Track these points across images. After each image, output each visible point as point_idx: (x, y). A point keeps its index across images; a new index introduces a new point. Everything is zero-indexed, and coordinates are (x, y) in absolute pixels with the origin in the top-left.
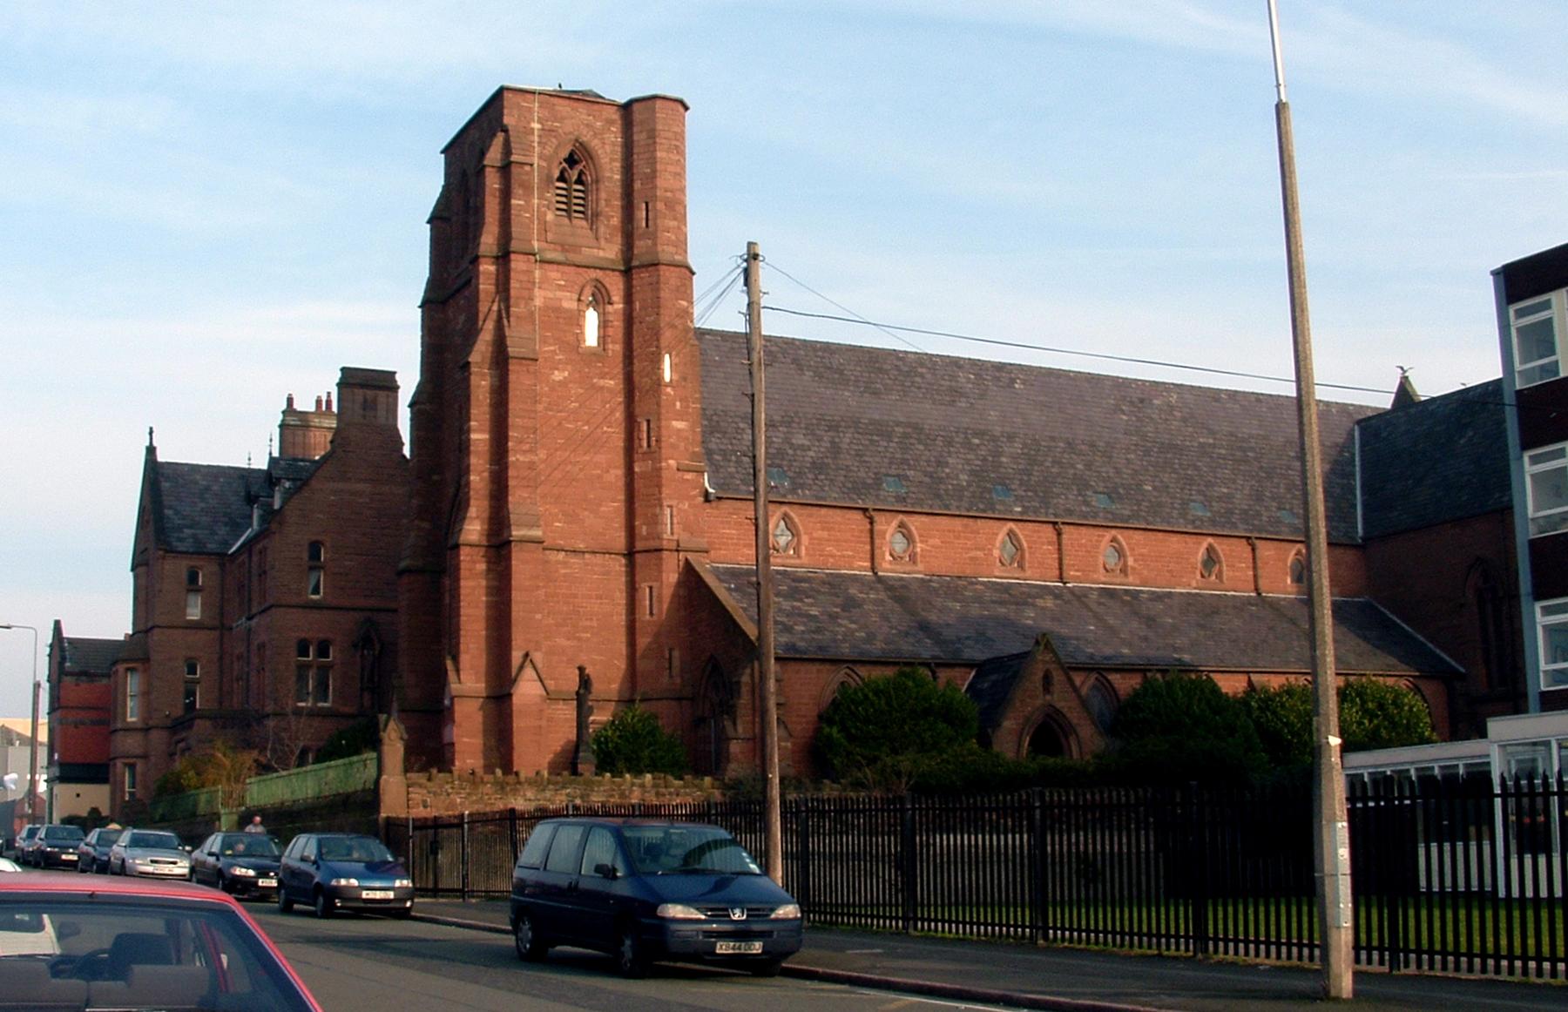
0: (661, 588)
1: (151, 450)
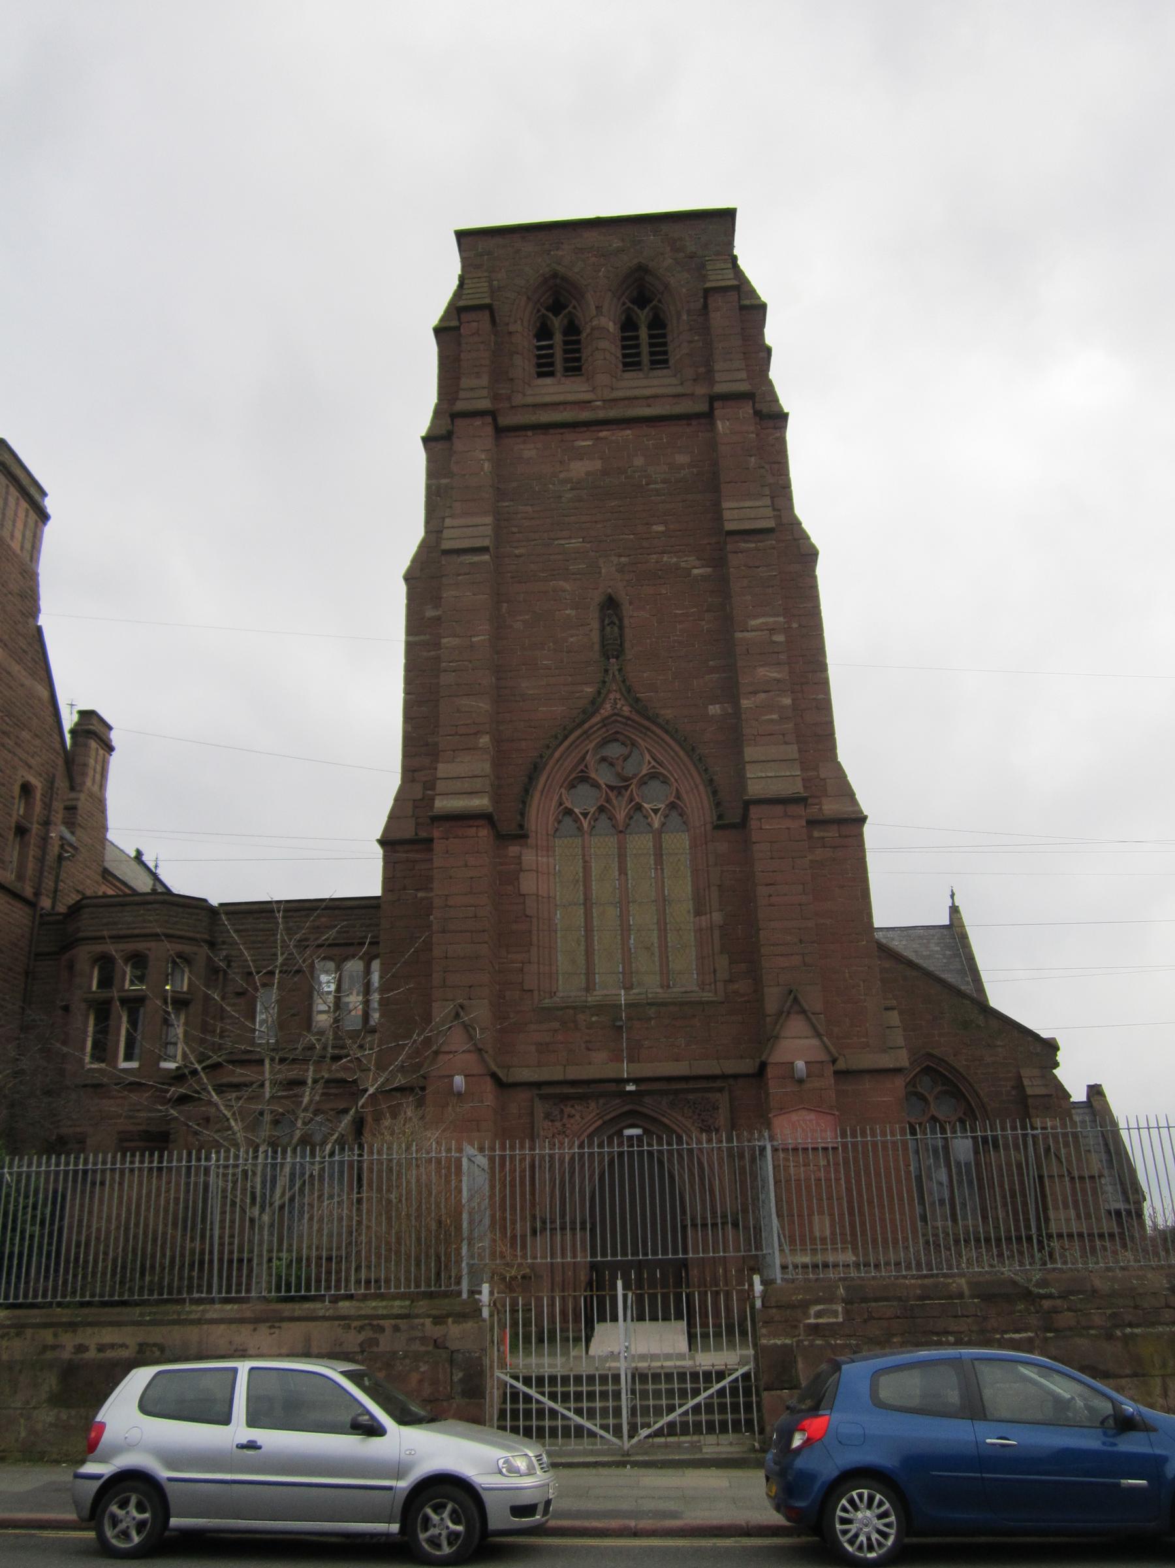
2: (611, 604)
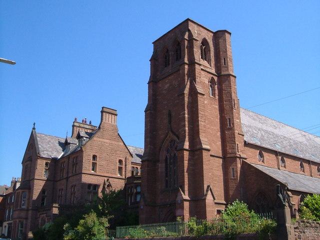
1: (34, 128)
2: (170, 115)
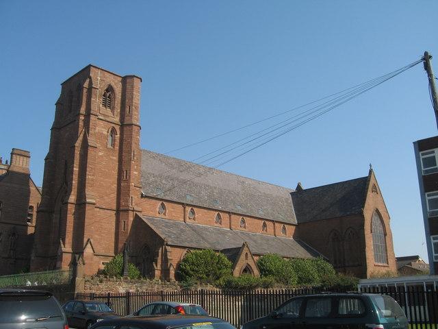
0: (128, 222)
